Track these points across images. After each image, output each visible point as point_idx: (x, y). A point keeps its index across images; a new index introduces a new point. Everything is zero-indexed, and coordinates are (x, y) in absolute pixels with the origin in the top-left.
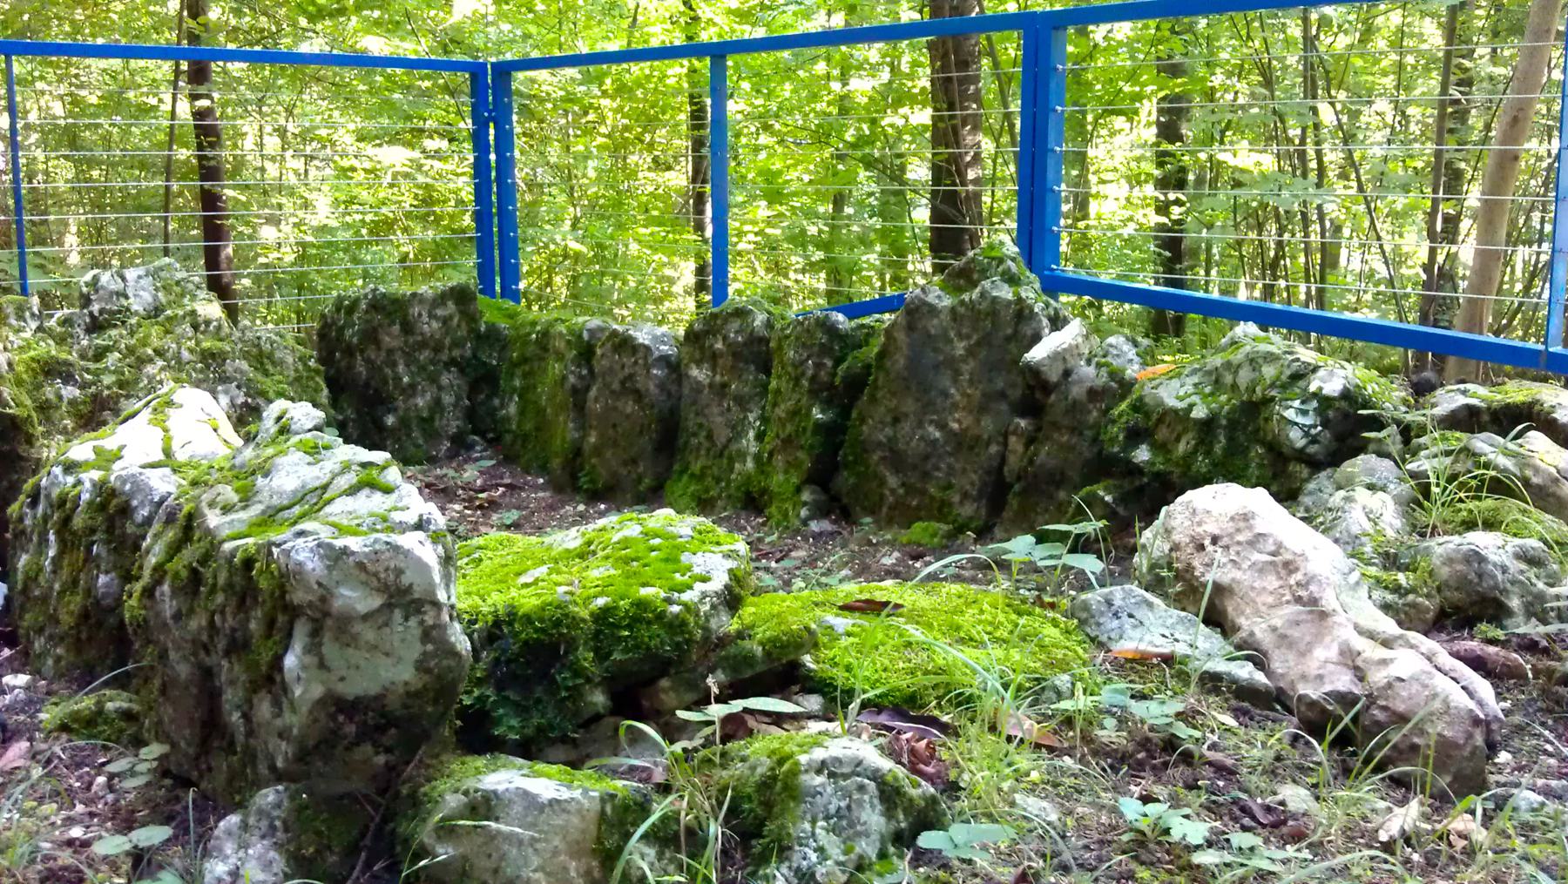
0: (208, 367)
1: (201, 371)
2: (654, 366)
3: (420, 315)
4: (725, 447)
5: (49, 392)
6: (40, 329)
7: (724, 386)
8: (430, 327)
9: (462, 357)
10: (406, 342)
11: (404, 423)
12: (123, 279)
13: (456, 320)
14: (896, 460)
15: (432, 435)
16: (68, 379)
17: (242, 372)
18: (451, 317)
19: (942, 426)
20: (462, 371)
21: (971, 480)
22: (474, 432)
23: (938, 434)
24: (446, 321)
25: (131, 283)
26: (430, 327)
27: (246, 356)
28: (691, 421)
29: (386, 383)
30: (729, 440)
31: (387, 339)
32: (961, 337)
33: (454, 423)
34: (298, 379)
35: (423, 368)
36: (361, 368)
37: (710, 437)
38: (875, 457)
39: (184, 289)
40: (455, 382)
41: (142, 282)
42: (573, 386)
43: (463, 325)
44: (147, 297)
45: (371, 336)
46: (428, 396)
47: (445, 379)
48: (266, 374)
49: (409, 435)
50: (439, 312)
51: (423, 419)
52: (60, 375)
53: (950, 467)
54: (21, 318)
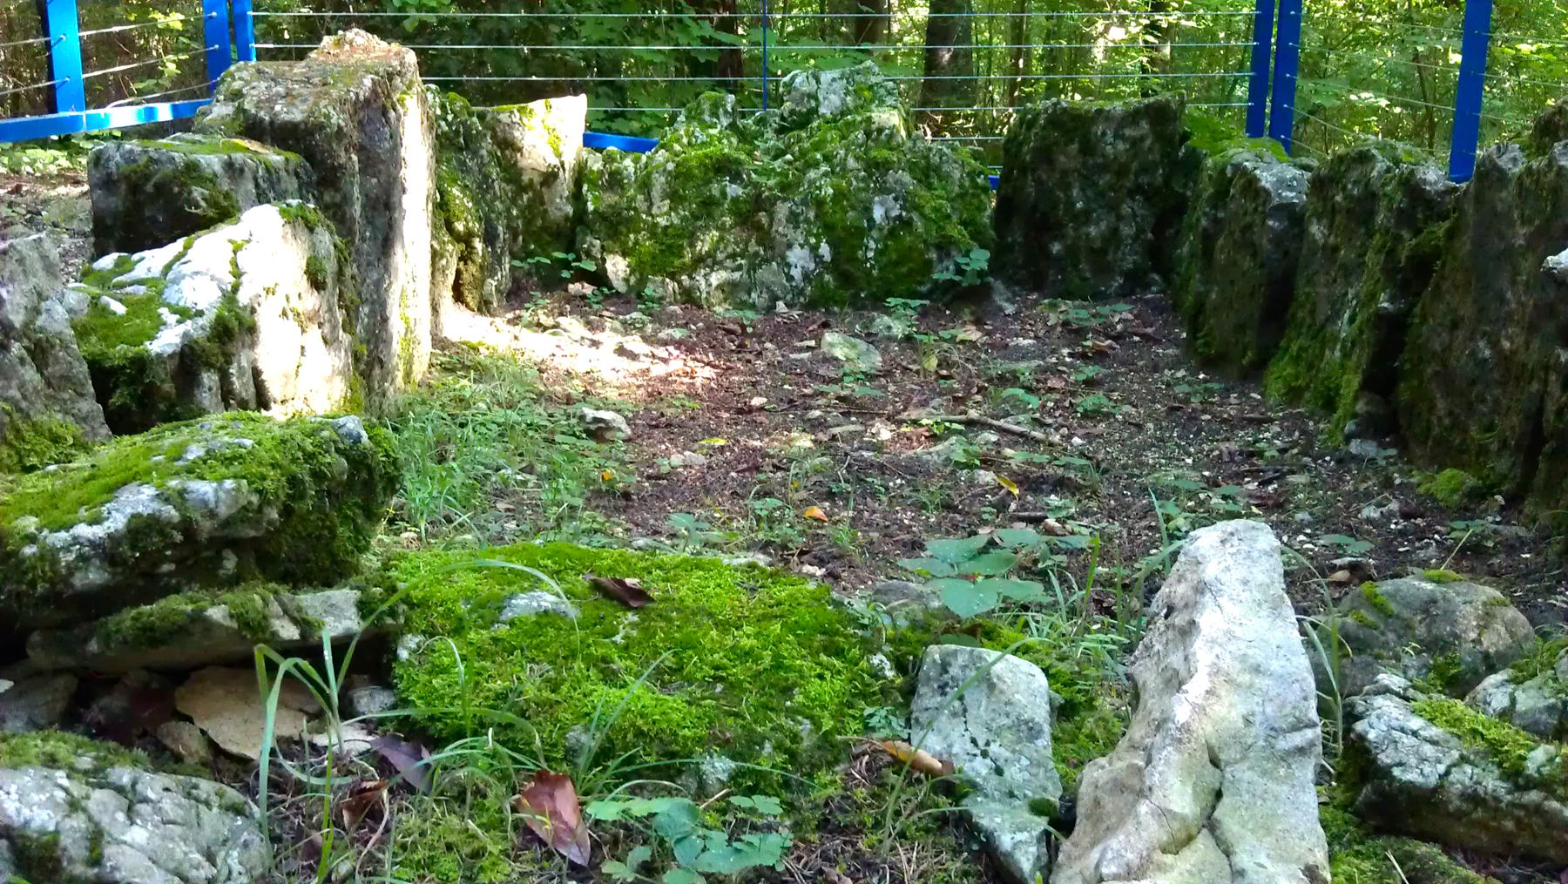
0: (870, 175)
1: (863, 179)
2: (1270, 216)
3: (1104, 134)
4: (1323, 327)
5: (715, 189)
6: (732, 126)
7: (1335, 249)
8: (1114, 148)
9: (1149, 185)
10: (1084, 165)
11: (1072, 252)
12: (818, 82)
13: (1148, 142)
14: (1446, 378)
15: (1103, 268)
16: (736, 178)
17: (903, 184)
18: (1142, 139)
19: (1494, 344)
20: (1147, 199)
21: (1511, 424)
22: (1156, 269)
23: (1487, 353)
24: (1135, 143)
25: (824, 86)
26: (1114, 148)
27: (912, 168)
28: (1302, 290)
29: (1055, 207)
30: (1327, 320)
31: (1062, 159)
32: (1525, 221)
33: (1130, 259)
34: (962, 196)
35: (1102, 194)
36: (1031, 189)
37: (1312, 312)
38: (1429, 371)
39: (875, 93)
40: (1140, 212)
41: (835, 85)
42: (1205, 230)
43: (1157, 146)
44: (835, 100)
45: (1045, 155)
46: (1103, 225)
47: (1126, 209)
48: (930, 187)
49: (1075, 266)
50: (1128, 132)
51: (1093, 250)
52: (729, 173)
53: (1496, 401)
54: (715, 114)
